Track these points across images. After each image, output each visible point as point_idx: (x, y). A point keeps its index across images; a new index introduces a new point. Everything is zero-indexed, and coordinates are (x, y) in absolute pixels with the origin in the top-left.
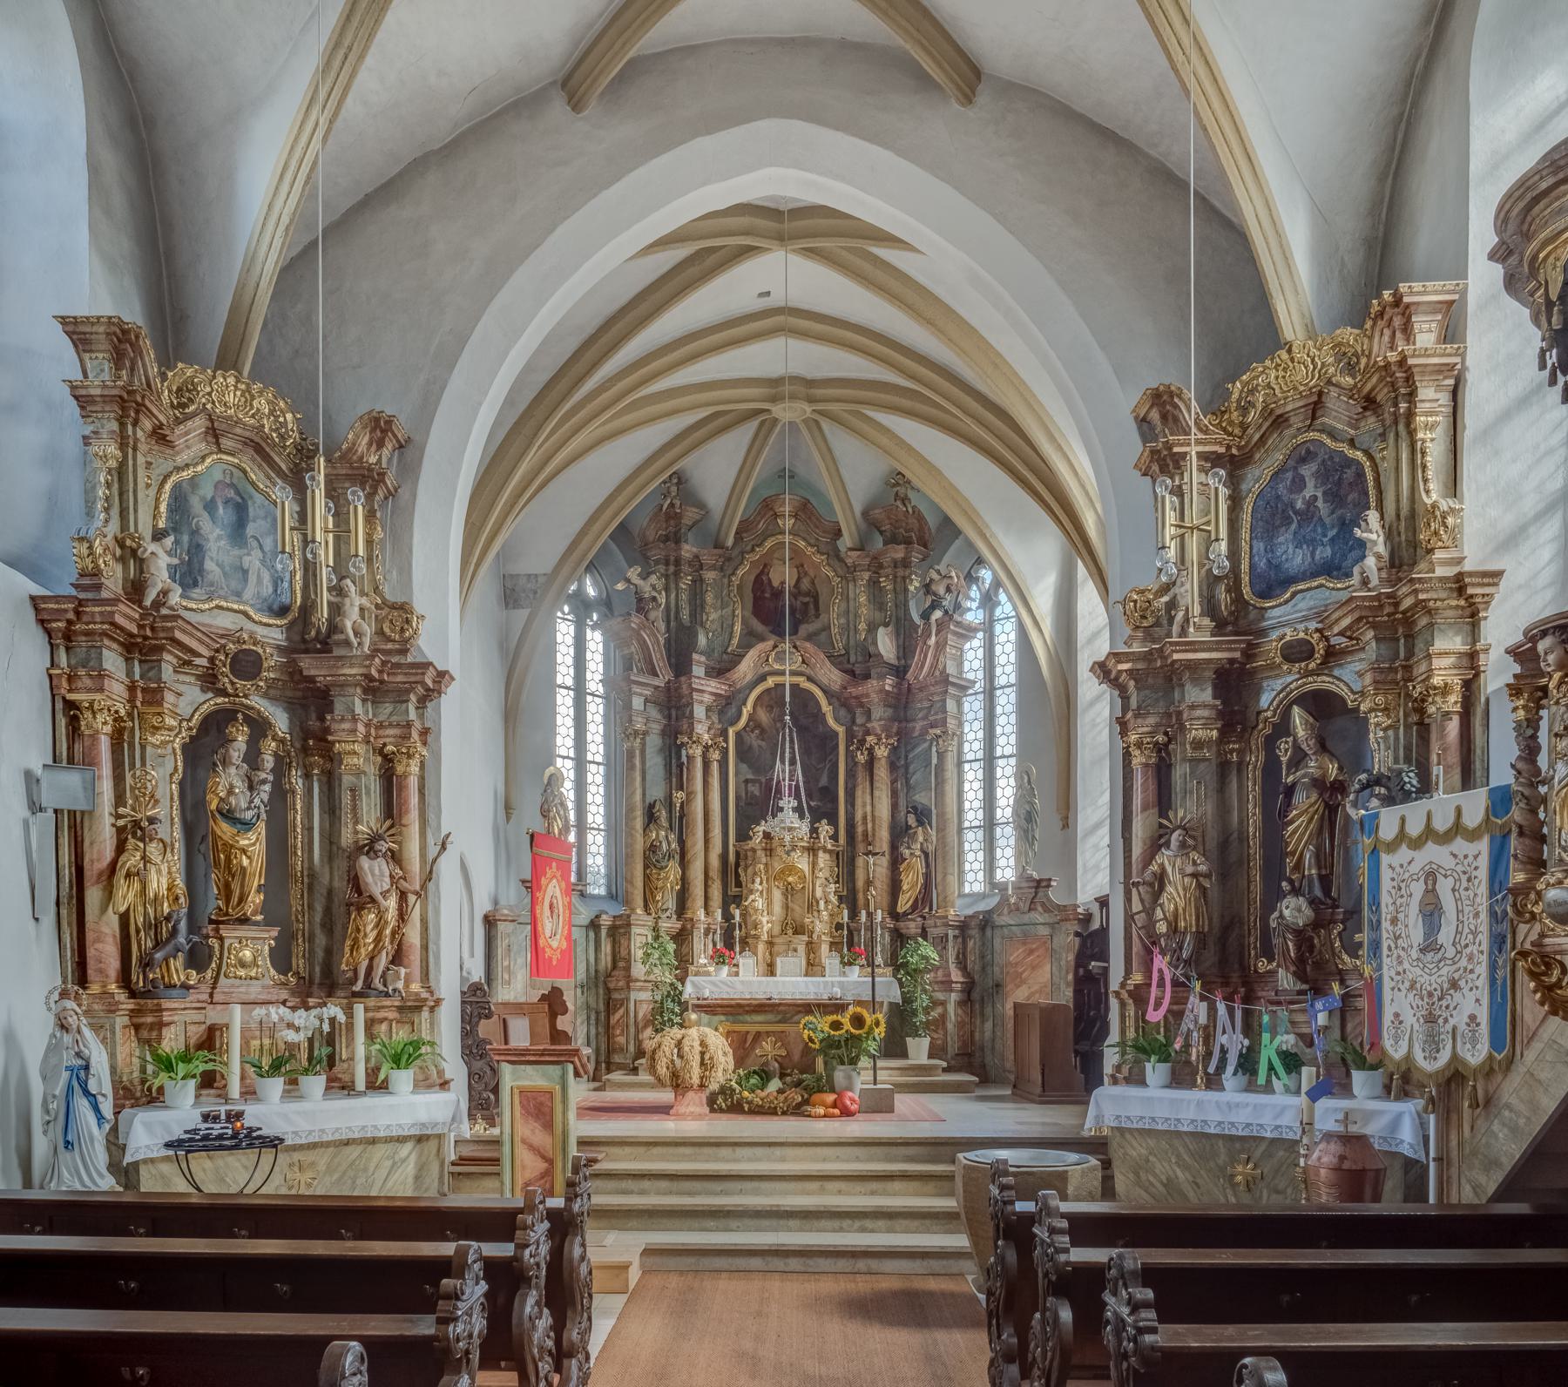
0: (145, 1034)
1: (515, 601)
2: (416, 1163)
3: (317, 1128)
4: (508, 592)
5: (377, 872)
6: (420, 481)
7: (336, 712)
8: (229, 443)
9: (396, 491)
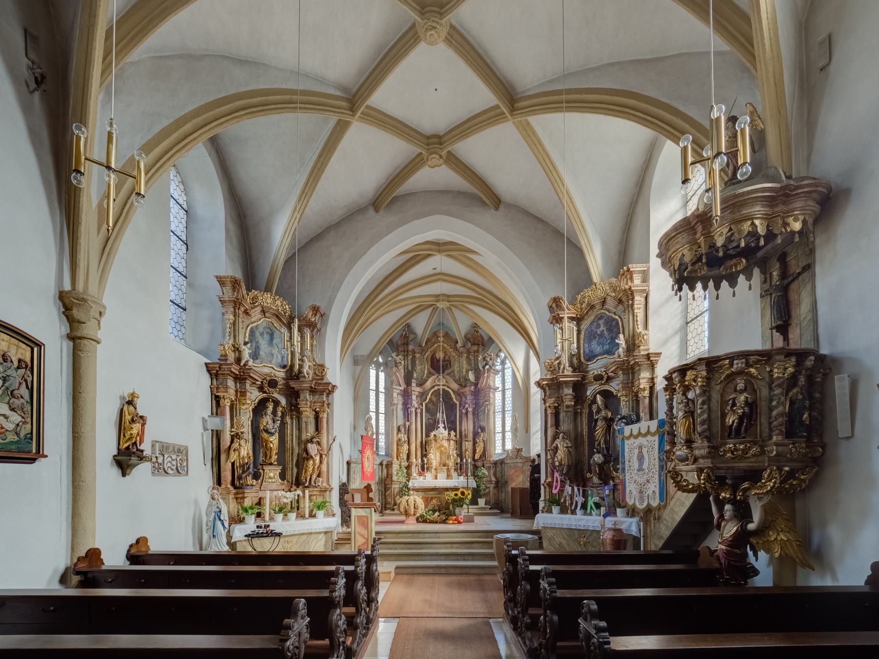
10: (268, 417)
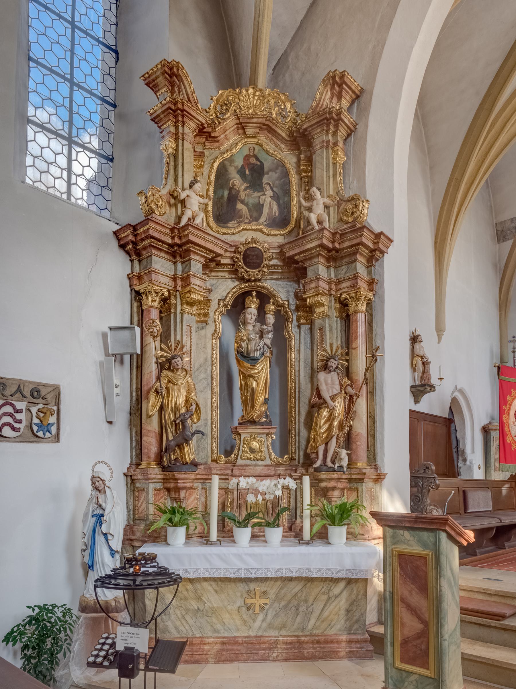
0: (173, 494)
1: (504, 237)
2: (347, 600)
3: (263, 567)
4: (499, 233)
5: (329, 382)
6: (370, 115)
7: (309, 277)
8: (251, 130)
9: (356, 129)
10: (250, 327)
